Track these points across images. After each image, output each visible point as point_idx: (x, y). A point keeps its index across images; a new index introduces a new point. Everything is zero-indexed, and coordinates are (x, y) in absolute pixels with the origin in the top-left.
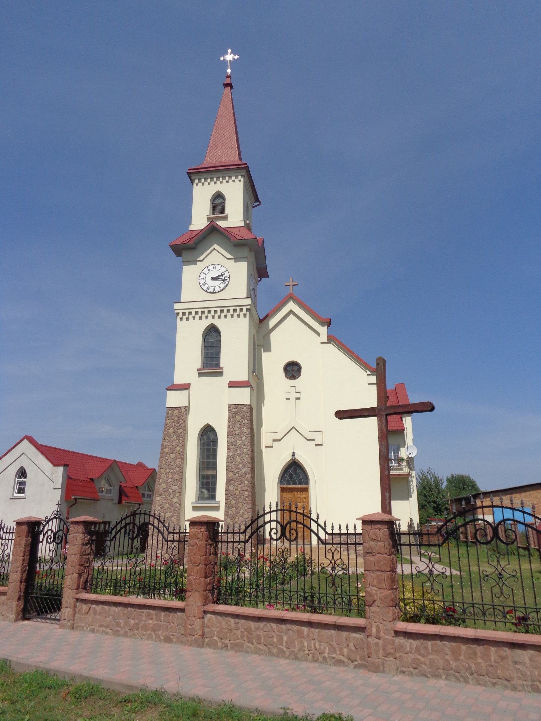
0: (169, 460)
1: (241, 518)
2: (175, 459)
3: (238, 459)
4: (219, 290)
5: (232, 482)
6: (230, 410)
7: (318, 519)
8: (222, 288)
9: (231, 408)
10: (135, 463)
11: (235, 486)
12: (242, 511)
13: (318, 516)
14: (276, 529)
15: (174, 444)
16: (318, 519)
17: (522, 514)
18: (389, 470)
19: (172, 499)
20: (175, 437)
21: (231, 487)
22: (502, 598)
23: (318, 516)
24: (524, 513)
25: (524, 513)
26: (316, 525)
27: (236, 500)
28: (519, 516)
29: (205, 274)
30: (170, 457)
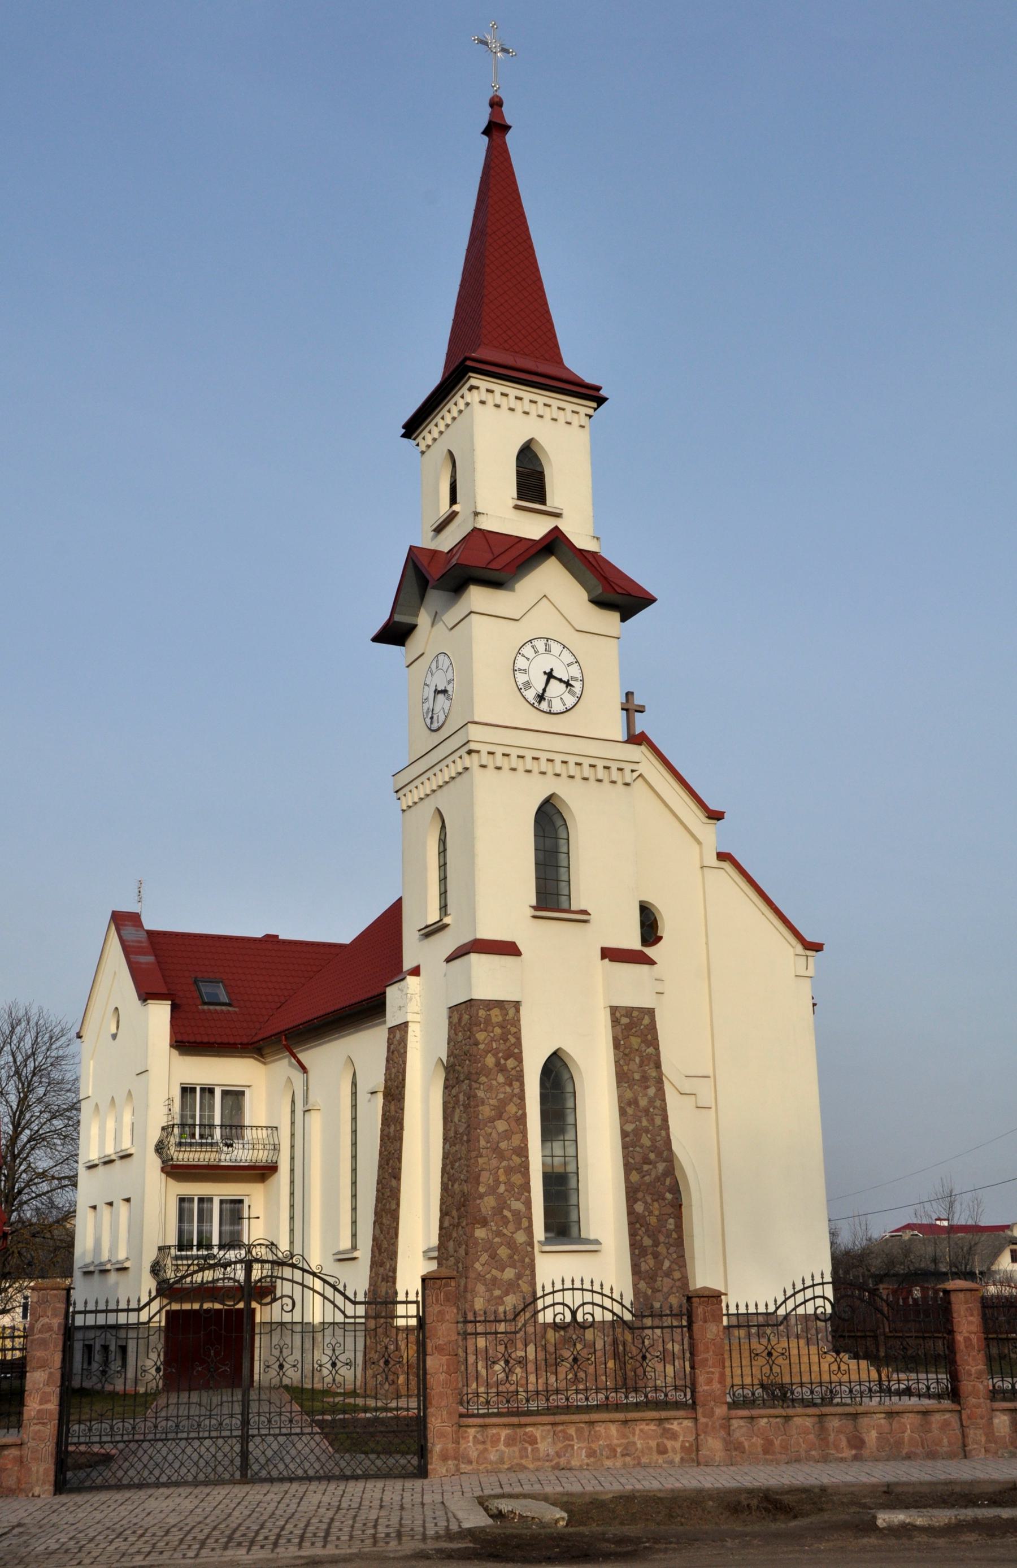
0: (494, 1135)
1: (666, 1280)
2: (507, 1135)
3: (646, 1140)
4: (562, 709)
5: (640, 1195)
6: (615, 1021)
7: (622, 1299)
8: (569, 705)
9: (618, 1015)
10: (259, 935)
11: (646, 1203)
12: (667, 1264)
13: (621, 1295)
14: (824, 1307)
15: (501, 1096)
16: (622, 1299)
17: (610, 1300)
18: (67, 1445)
19: (513, 1233)
20: (501, 1079)
21: (639, 1207)
22: (840, 1375)
23: (621, 1295)
24: (613, 1299)
25: (613, 1299)
26: (336, 1303)
27: (653, 1235)
28: (598, 1299)
29: (528, 659)
30: (495, 1128)
